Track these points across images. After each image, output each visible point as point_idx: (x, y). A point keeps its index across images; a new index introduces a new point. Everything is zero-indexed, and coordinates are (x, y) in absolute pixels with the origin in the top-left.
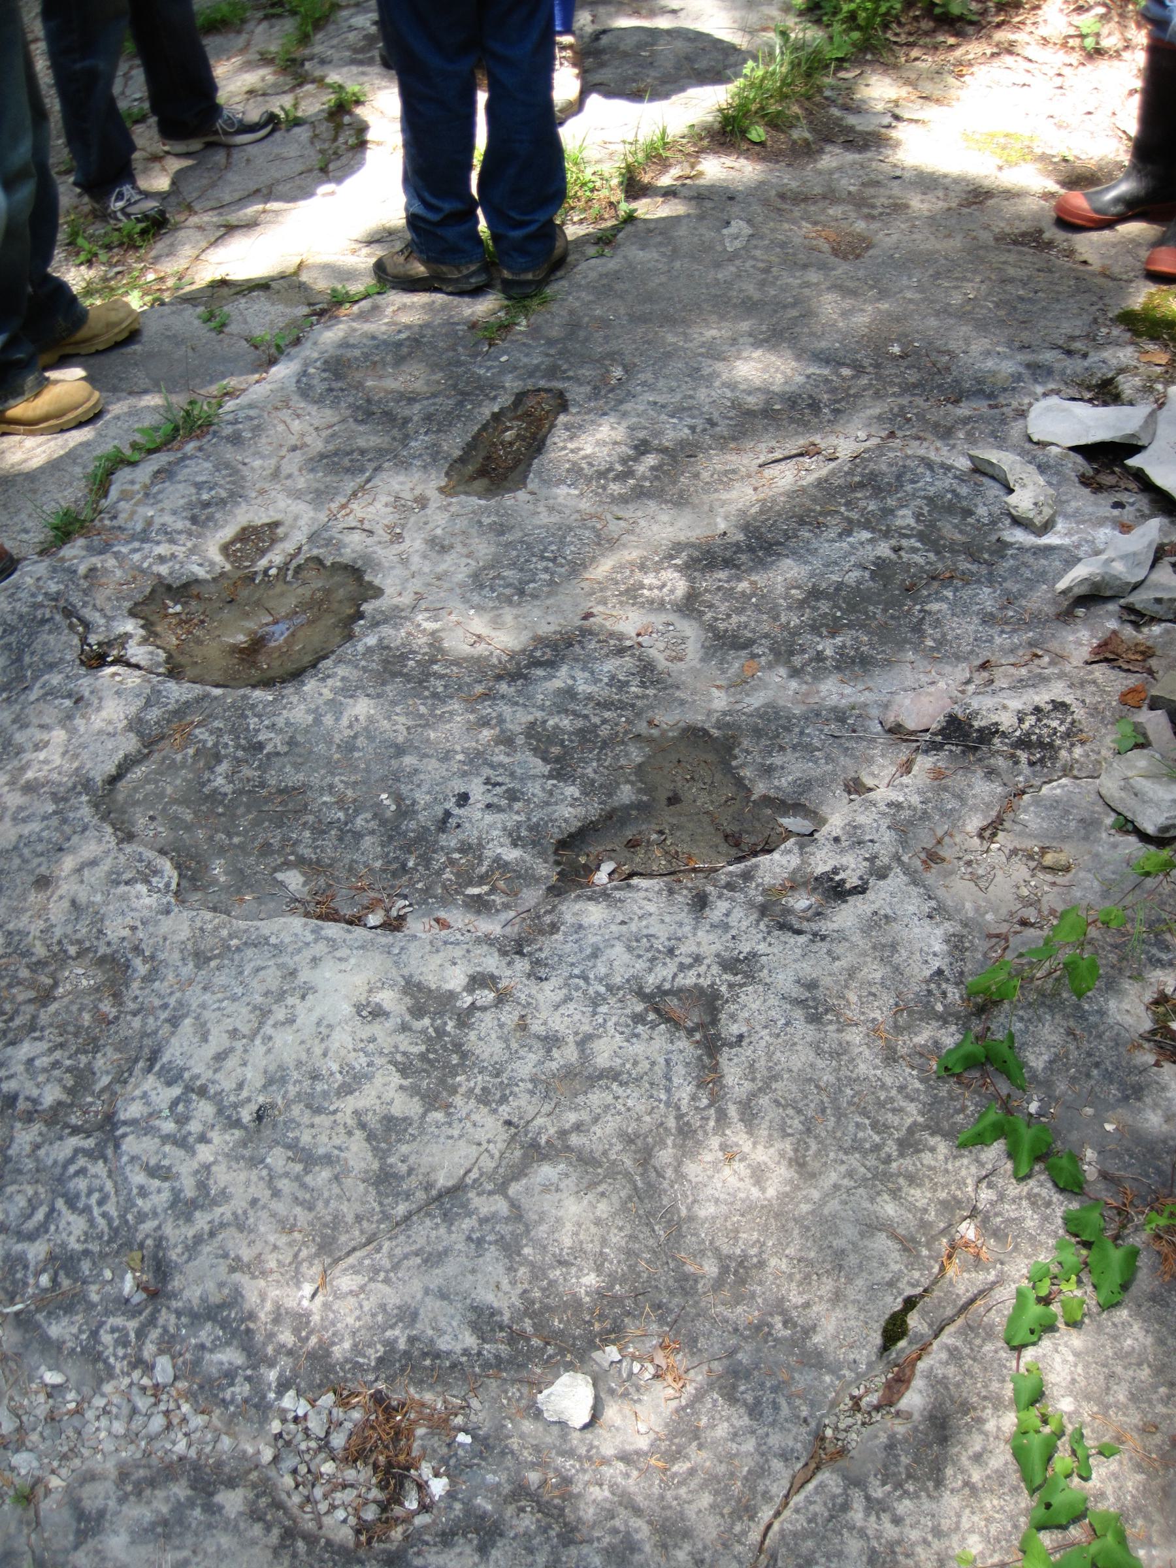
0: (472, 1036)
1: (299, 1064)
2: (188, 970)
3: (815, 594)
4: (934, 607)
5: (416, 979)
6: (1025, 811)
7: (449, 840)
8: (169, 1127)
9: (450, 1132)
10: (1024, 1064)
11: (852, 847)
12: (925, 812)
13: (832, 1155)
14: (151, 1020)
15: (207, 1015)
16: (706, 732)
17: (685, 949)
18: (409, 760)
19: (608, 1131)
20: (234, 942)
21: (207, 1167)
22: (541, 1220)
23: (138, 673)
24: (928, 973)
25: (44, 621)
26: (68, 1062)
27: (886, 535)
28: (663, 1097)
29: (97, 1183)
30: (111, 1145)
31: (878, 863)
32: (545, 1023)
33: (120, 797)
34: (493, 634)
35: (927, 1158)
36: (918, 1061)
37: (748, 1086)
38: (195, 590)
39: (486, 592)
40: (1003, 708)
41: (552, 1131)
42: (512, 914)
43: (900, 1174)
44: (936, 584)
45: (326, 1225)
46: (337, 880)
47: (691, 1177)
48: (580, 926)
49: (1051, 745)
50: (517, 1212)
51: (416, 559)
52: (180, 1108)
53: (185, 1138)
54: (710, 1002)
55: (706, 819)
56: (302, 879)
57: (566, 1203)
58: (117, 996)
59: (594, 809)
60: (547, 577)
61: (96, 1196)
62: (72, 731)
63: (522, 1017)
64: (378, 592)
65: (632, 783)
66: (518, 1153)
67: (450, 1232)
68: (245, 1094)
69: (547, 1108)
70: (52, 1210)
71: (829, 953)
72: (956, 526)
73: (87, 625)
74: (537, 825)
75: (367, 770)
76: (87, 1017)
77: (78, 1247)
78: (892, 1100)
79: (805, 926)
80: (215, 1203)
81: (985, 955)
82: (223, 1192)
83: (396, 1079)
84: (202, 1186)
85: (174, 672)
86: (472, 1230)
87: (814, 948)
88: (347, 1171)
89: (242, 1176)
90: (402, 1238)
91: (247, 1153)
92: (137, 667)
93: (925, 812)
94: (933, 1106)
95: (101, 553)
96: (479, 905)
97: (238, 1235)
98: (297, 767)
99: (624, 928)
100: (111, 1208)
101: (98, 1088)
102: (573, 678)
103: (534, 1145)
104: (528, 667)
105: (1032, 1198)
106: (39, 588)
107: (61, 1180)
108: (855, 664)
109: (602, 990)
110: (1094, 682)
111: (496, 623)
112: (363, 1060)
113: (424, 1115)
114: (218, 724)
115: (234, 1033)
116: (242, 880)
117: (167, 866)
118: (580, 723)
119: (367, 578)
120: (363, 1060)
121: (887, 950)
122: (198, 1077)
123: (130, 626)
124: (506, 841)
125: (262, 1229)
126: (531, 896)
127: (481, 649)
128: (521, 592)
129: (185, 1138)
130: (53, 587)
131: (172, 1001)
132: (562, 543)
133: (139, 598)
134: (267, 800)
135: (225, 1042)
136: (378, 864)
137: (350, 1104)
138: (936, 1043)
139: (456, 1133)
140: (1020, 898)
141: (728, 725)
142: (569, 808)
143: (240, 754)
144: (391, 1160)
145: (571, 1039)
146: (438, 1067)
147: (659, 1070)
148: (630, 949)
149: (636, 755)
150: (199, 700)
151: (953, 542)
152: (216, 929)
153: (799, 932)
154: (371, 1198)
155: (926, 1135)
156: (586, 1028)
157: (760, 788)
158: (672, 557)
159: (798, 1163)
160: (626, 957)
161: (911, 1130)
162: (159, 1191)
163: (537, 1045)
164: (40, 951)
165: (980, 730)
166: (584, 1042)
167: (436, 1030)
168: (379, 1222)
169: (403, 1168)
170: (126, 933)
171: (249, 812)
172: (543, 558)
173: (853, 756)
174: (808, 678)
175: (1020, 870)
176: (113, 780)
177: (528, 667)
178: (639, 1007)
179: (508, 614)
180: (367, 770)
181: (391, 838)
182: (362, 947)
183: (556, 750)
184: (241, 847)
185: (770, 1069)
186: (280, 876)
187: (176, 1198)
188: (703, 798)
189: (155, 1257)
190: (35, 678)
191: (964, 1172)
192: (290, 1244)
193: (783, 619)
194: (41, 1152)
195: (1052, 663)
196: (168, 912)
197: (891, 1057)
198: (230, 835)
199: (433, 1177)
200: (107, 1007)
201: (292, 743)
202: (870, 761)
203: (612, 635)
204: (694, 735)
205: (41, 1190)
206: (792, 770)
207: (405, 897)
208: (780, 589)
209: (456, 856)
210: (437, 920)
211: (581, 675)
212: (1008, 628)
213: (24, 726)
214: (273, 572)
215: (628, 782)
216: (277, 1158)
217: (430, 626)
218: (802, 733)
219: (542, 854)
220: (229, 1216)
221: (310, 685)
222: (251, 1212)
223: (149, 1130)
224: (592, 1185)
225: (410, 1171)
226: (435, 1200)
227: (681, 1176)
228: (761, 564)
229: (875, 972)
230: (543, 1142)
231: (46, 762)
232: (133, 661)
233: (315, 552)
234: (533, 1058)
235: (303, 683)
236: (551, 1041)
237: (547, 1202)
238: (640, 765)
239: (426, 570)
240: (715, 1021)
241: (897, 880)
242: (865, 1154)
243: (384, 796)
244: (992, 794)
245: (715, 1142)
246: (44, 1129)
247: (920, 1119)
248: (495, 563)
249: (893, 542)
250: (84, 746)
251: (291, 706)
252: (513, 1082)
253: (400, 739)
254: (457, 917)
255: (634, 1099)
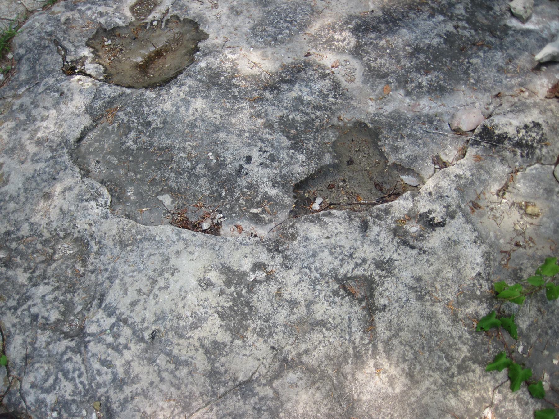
0: (255, 298)
1: (171, 311)
2: (117, 250)
3: (417, 50)
4: (474, 61)
5: (227, 265)
6: (519, 182)
7: (243, 182)
8: (110, 339)
9: (245, 352)
10: (517, 326)
11: (438, 199)
12: (472, 181)
13: (427, 372)
14: (100, 277)
15: (127, 279)
16: (366, 125)
17: (358, 254)
18: (222, 135)
19: (321, 354)
20: (139, 237)
21: (128, 363)
22: (289, 400)
23: (90, 79)
24: (474, 274)
25: (45, 47)
26: (61, 298)
27: (451, 18)
28: (347, 337)
29: (77, 366)
30: (83, 345)
31: (450, 209)
32: (290, 294)
33: (83, 149)
34: (262, 62)
35: (471, 375)
36: (468, 322)
37: (388, 333)
38: (117, 32)
39: (258, 38)
40: (509, 124)
41: (294, 353)
42: (273, 225)
43: (457, 384)
44: (475, 48)
45: (186, 397)
46: (188, 201)
47: (360, 380)
48: (307, 238)
49: (532, 146)
50: (277, 396)
51: (224, 18)
52: (115, 329)
53: (118, 346)
54: (369, 284)
55: (365, 173)
56: (171, 200)
57: (301, 393)
58: (84, 261)
59: (312, 168)
60: (288, 32)
61: (77, 373)
62: (59, 111)
63: (279, 289)
64: (206, 36)
65: (331, 153)
66: (277, 364)
67: (245, 404)
68: (146, 325)
69: (291, 341)
70: (57, 378)
71: (428, 261)
72: (484, 16)
73: (66, 50)
74: (285, 175)
75: (202, 139)
76: (69, 271)
77: (70, 398)
78: (455, 344)
79: (416, 243)
80: (133, 382)
81: (500, 263)
82: (137, 376)
83: (219, 322)
84: (127, 372)
85: (108, 79)
86: (256, 404)
87: (420, 258)
88: (196, 369)
89: (146, 369)
90: (222, 405)
91: (147, 355)
92: (90, 76)
93: (472, 181)
94: (475, 347)
95: (72, 10)
96: (257, 219)
97: (144, 400)
98: (168, 136)
99: (328, 240)
100: (84, 379)
101: (76, 312)
102: (301, 91)
103: (285, 360)
104: (279, 82)
105: (519, 400)
106: (42, 29)
107: (60, 362)
108: (438, 91)
109: (318, 276)
110: (551, 110)
111: (264, 56)
112: (203, 311)
113: (232, 342)
114: (129, 110)
115: (139, 291)
116: (142, 200)
117: (105, 191)
118: (305, 118)
119: (201, 28)
120: (203, 311)
121: (455, 260)
122: (122, 314)
123: (86, 52)
124: (270, 184)
125: (156, 398)
126: (283, 215)
127: (256, 70)
128: (275, 40)
129: (118, 346)
130: (49, 29)
131: (110, 268)
132: (295, 13)
133: (91, 36)
134: (153, 154)
135: (135, 296)
136: (207, 193)
137: (196, 334)
138: (477, 313)
139: (248, 353)
140: (515, 230)
141: (376, 122)
142: (300, 169)
143: (140, 127)
144: (216, 365)
145: (303, 303)
146: (238, 315)
147: (346, 322)
148: (331, 253)
149: (332, 136)
150: (120, 96)
151: (483, 25)
152: (130, 229)
153: (413, 247)
154: (207, 384)
155: (470, 363)
156: (310, 298)
157: (392, 159)
158: (347, 23)
159: (410, 375)
160: (330, 258)
161: (464, 360)
162: (106, 374)
163: (286, 305)
164: (46, 235)
165: (499, 136)
166: (309, 305)
167: (237, 294)
168: (211, 396)
169: (223, 370)
170: (87, 227)
171: (145, 160)
172: (286, 21)
173: (436, 143)
174: (414, 97)
175: (515, 215)
176: (79, 140)
177: (279, 82)
178: (336, 287)
179: (269, 51)
180: (202, 139)
181: (214, 179)
182: (200, 245)
183: (293, 132)
184: (141, 180)
185: (398, 325)
186: (160, 198)
187: (115, 378)
188: (364, 162)
189: (106, 405)
190: (42, 78)
191: (488, 384)
192: (169, 407)
193: (402, 63)
194: (51, 347)
195: (530, 96)
196: (106, 218)
197: (455, 320)
198: (136, 173)
199: (237, 375)
200: (79, 267)
201: (165, 122)
202: (445, 147)
203: (320, 66)
204: (360, 126)
205: (51, 367)
206: (407, 150)
207: (221, 212)
208: (401, 46)
209: (245, 190)
210: (237, 226)
211: (306, 90)
212: (509, 75)
213: (36, 106)
214: (155, 23)
215: (329, 152)
216: (162, 360)
217: (231, 57)
218: (412, 128)
219: (287, 192)
220: (139, 390)
221: (174, 90)
222: (150, 389)
223: (100, 341)
224: (313, 383)
225: (226, 371)
226: (237, 386)
227: (355, 379)
228: (391, 32)
229: (449, 273)
230: (289, 359)
231: (47, 128)
232: (88, 72)
233: (176, 12)
234: (284, 312)
235: (170, 88)
236: (294, 304)
237: (292, 393)
238: (334, 142)
239: (229, 24)
240: (372, 296)
241: (459, 220)
242: (442, 372)
243: (210, 154)
244: (504, 172)
245: (371, 363)
246: (52, 334)
247: (468, 354)
248: (262, 23)
249: (454, 23)
250: (65, 120)
251: (163, 102)
252: (275, 326)
253: (218, 123)
254: (247, 226)
255: (333, 338)
